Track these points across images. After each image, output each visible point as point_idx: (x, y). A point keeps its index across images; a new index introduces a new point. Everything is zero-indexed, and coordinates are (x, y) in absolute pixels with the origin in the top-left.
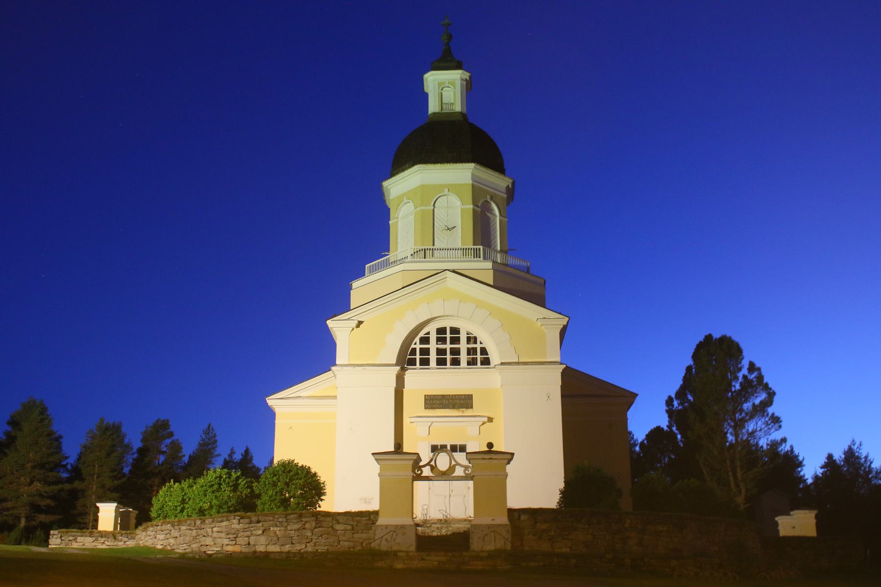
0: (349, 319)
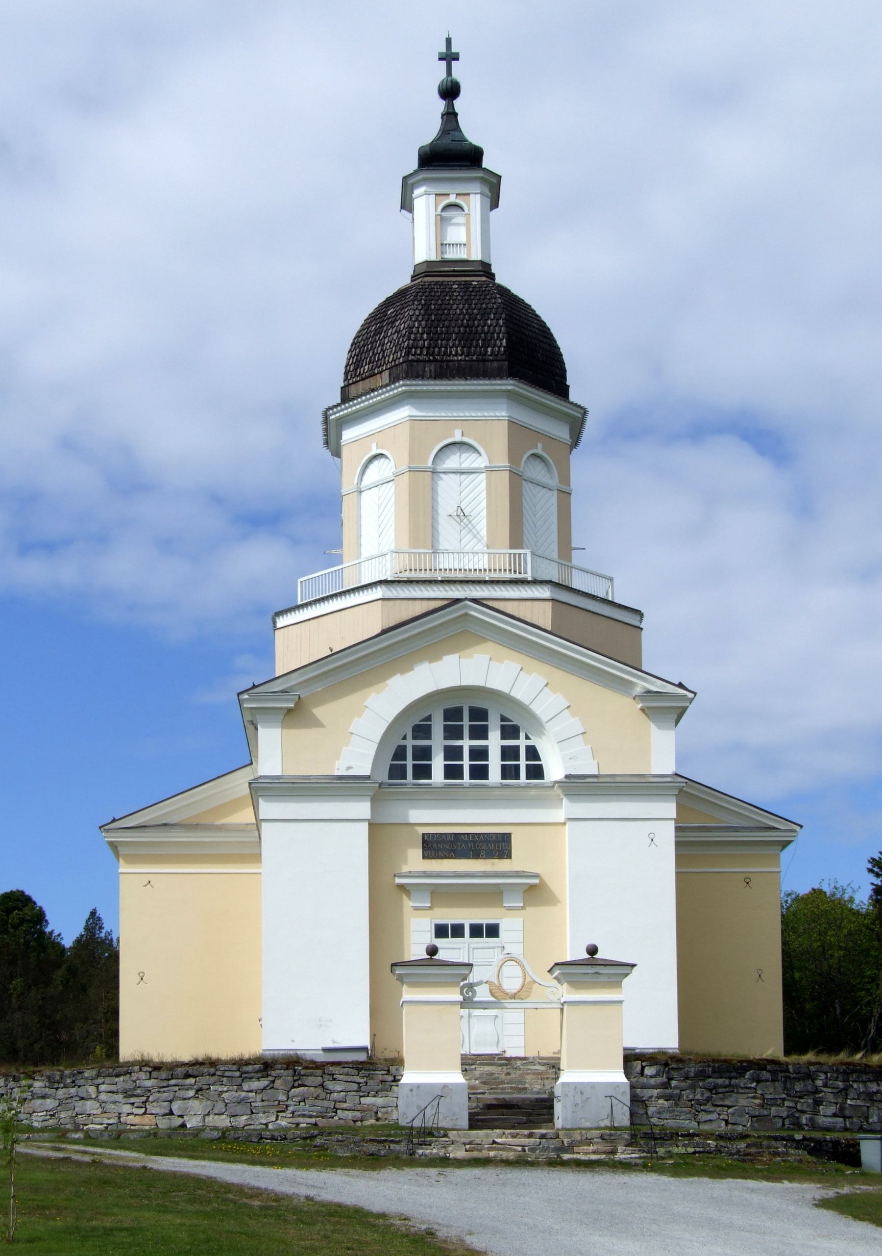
0: (283, 691)
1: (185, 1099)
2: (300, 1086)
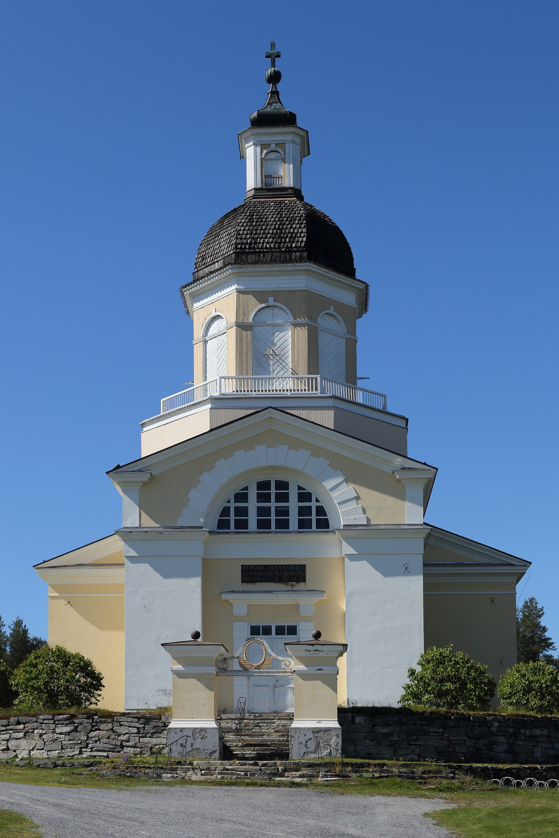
0: (140, 471)
1: (17, 739)
2: (96, 730)
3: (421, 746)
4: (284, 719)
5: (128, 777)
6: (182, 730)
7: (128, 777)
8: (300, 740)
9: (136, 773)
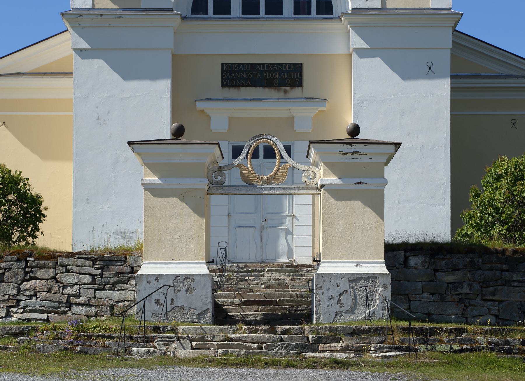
2: (31, 278)
3: (500, 302)
4: (276, 271)
5: (78, 352)
6: (157, 277)
7: (78, 352)
8: (330, 293)
9: (91, 346)
